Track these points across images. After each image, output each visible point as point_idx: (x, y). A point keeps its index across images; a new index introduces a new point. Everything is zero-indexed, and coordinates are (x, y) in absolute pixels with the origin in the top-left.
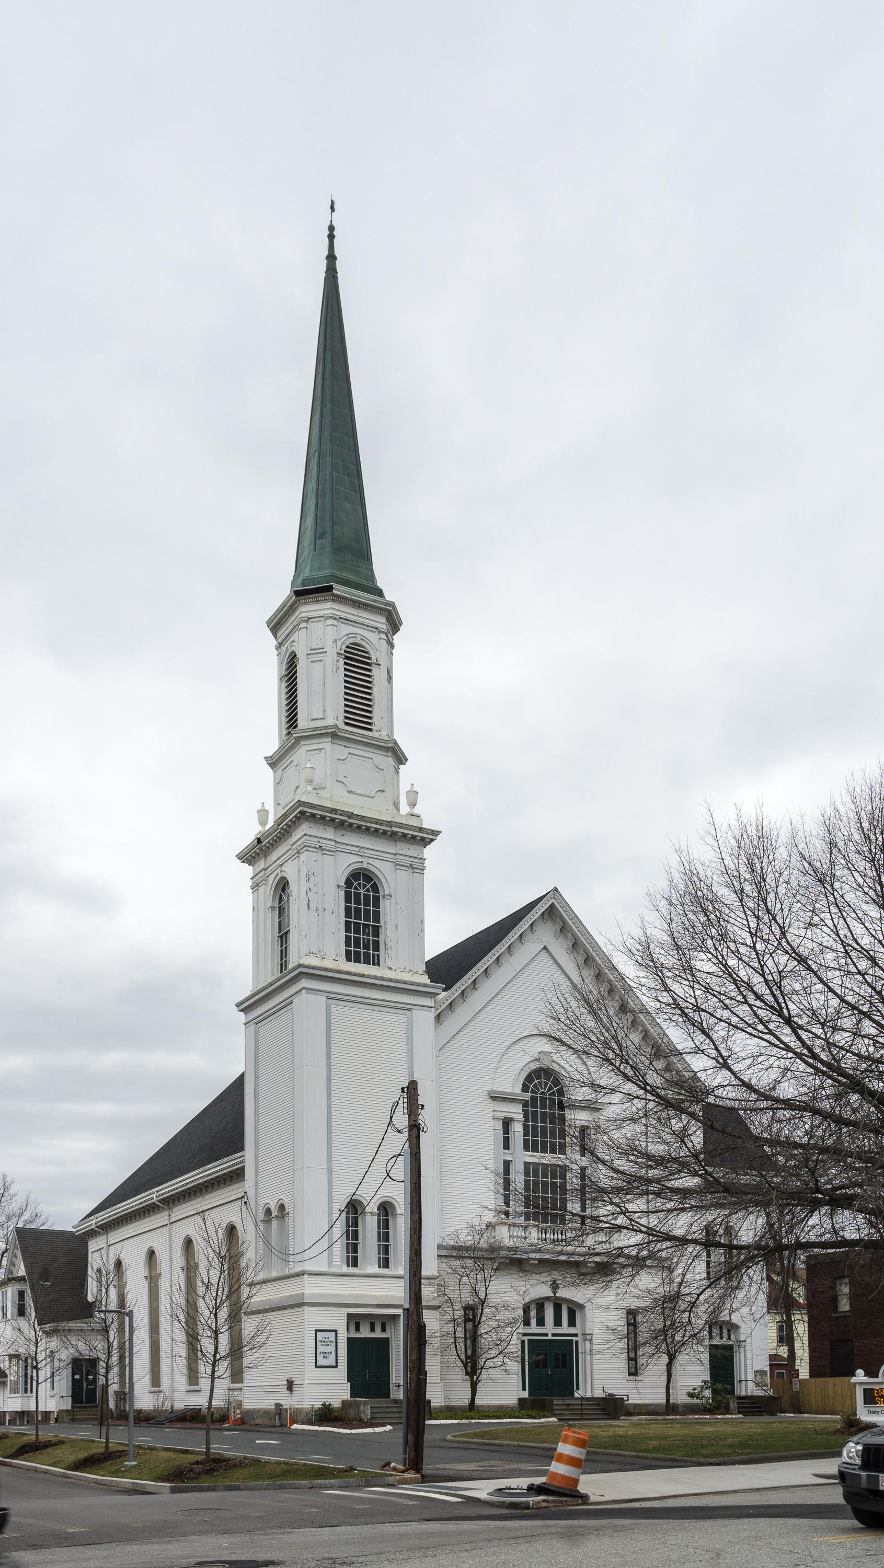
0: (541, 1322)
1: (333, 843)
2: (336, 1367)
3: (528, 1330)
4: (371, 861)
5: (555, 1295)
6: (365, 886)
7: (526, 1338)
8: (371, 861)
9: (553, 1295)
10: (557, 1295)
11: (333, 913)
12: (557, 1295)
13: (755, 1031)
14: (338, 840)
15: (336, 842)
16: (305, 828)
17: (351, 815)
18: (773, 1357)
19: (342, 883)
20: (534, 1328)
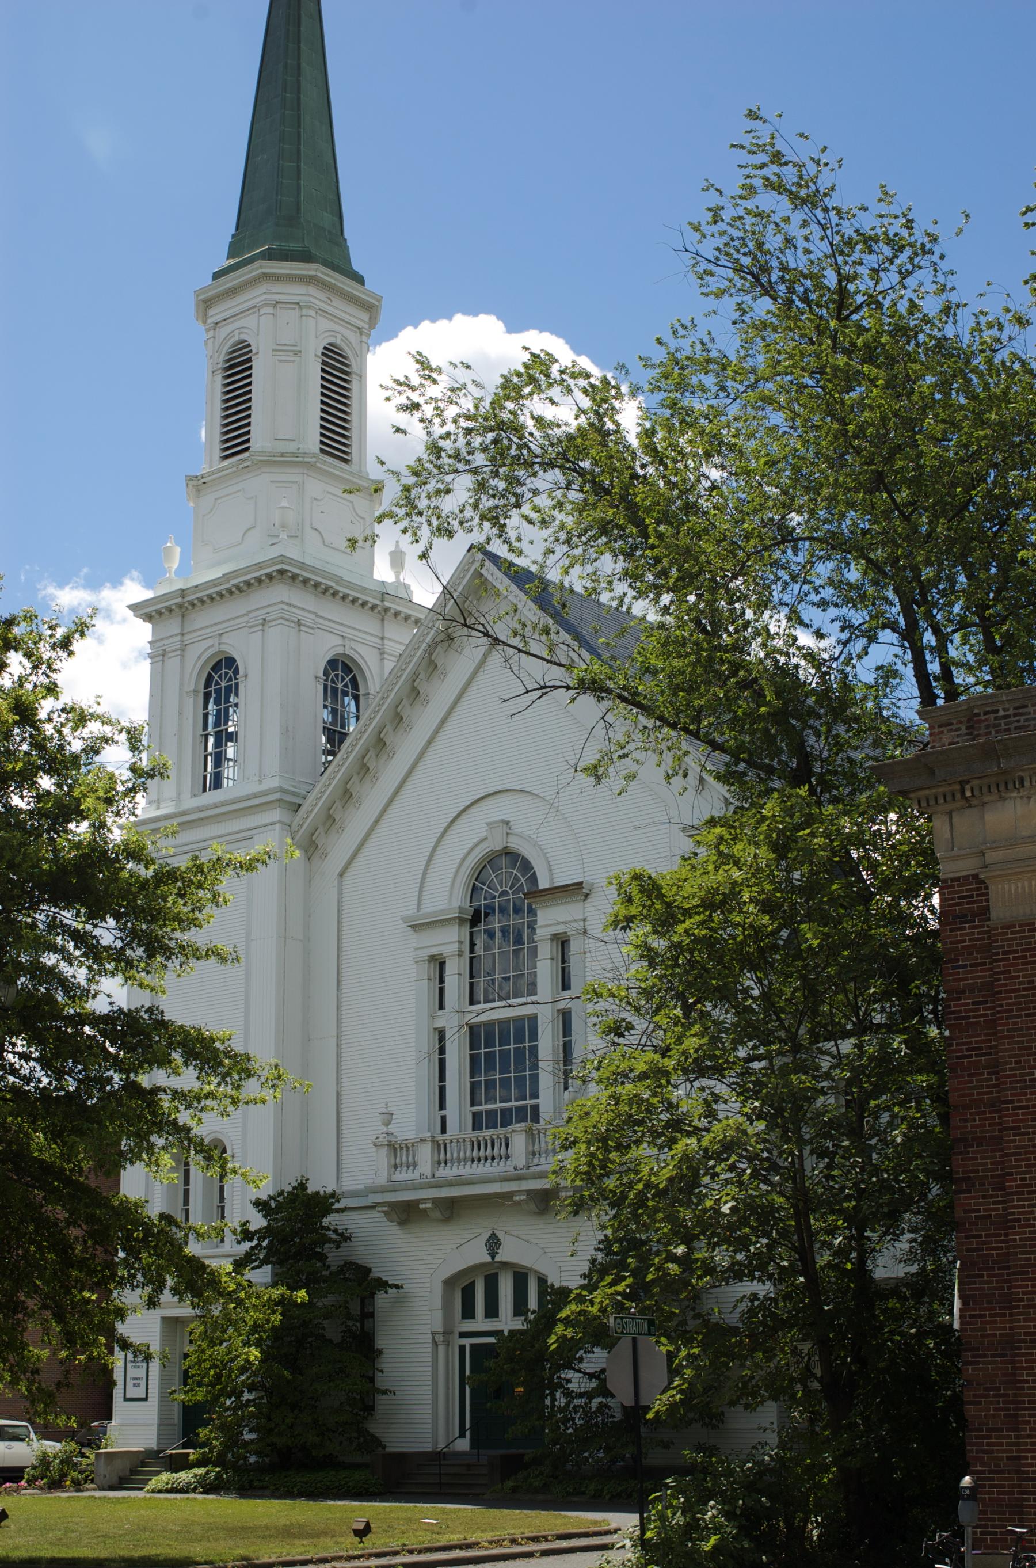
0: (492, 1311)
1: (313, 617)
2: (146, 1399)
3: (469, 1326)
4: (353, 644)
5: (493, 1258)
6: (343, 679)
7: (467, 1342)
8: (353, 644)
9: (489, 1259)
10: (498, 1258)
11: (801, 135)
12: (498, 1258)
13: (477, 942)
14: (320, 614)
15: (317, 616)
16: (280, 592)
17: (340, 580)
18: (593, 1261)
19: (321, 674)
20: (482, 1323)
